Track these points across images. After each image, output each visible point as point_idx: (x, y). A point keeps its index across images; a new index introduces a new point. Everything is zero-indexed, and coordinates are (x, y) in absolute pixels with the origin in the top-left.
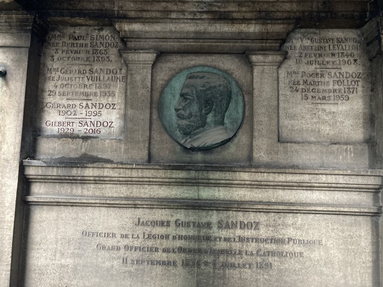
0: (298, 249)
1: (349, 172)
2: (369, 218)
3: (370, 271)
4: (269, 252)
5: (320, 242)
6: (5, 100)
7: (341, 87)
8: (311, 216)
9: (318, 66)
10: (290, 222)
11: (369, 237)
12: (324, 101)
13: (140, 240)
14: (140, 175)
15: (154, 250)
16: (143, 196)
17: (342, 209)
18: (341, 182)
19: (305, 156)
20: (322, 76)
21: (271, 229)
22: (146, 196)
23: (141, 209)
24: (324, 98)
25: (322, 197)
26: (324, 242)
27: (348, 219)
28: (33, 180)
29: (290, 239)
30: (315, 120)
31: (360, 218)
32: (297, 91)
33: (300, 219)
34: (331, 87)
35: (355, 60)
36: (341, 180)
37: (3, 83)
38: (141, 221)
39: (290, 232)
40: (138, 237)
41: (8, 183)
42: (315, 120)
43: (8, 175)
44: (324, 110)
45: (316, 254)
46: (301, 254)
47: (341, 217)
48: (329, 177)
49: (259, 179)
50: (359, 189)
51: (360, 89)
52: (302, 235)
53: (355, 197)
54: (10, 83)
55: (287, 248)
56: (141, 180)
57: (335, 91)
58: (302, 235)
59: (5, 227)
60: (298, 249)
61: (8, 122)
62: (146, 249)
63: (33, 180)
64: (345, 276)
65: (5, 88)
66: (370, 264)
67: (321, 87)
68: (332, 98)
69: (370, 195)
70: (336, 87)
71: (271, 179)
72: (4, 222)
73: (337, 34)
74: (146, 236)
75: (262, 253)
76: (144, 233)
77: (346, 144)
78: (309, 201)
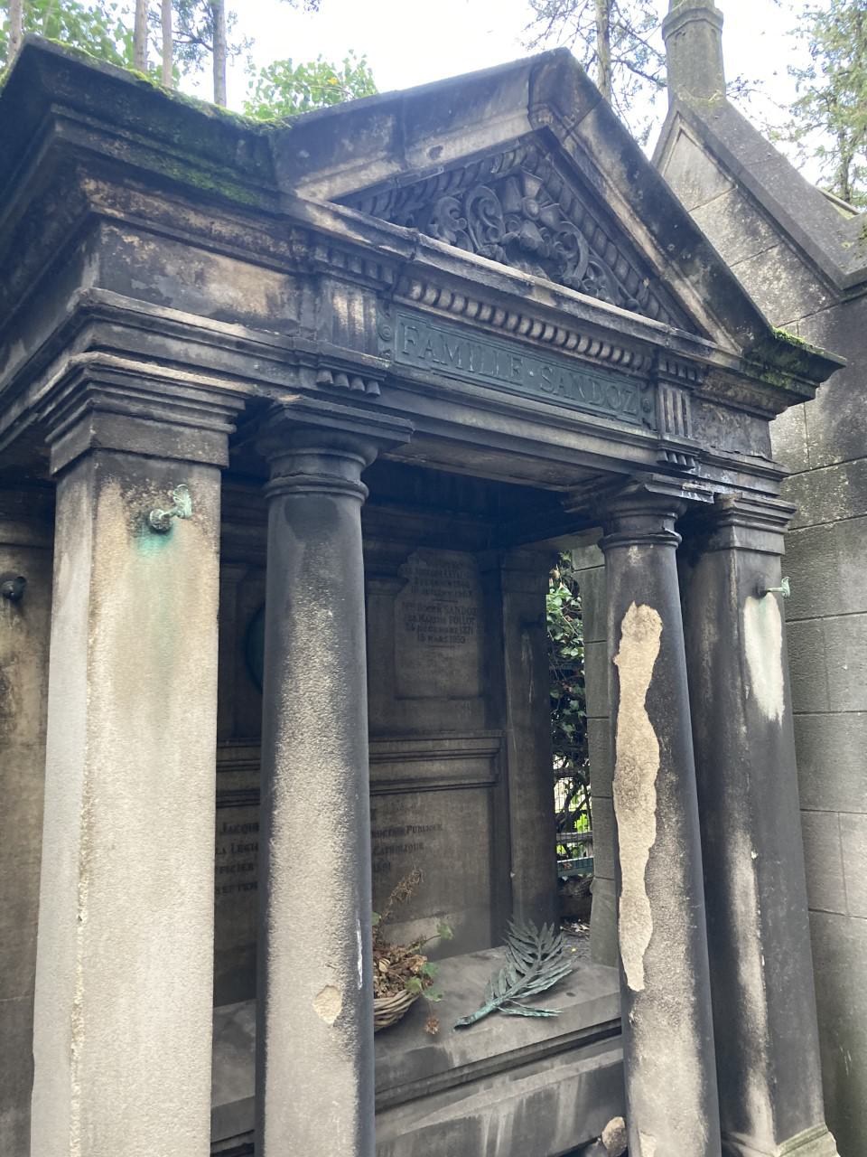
0: (418, 839)
1: (472, 735)
2: (485, 790)
3: (487, 854)
4: (387, 848)
5: (439, 826)
6: (18, 640)
7: (458, 626)
8: (431, 794)
9: (434, 597)
10: (409, 805)
11: (486, 813)
12: (441, 644)
13: (227, 856)
14: (234, 756)
15: (247, 867)
16: (232, 788)
17: (463, 782)
18: (464, 747)
19: (426, 717)
20: (439, 610)
21: (389, 816)
22: (238, 787)
23: (227, 809)
24: (441, 640)
25: (443, 768)
26: (443, 827)
27: (468, 793)
28: (621, 514)
29: (409, 827)
30: (432, 668)
31: (477, 792)
32: (413, 629)
33: (420, 800)
34: (447, 625)
35: (470, 592)
36: (464, 745)
37: (14, 610)
38: (228, 825)
39: (410, 818)
40: (224, 852)
41: (32, 784)
42: (432, 668)
43: (31, 771)
44: (440, 655)
45: (436, 844)
46: (421, 844)
47: (460, 792)
48: (452, 742)
49: (381, 750)
50: (477, 755)
51: (475, 629)
52: (421, 822)
53: (460, 766)
54: (28, 610)
55: (408, 839)
56: (232, 763)
57: (452, 630)
58: (421, 822)
59: (31, 860)
60: (418, 839)
61: (25, 679)
62: (236, 869)
63: (621, 514)
64: (464, 866)
65: (16, 619)
66: (487, 847)
67: (437, 625)
68: (448, 639)
69: (487, 761)
70: (453, 625)
71: (394, 749)
72: (29, 852)
73: (452, 556)
74: (236, 849)
75: (379, 850)
76: (233, 845)
77: (463, 698)
78: (429, 775)
